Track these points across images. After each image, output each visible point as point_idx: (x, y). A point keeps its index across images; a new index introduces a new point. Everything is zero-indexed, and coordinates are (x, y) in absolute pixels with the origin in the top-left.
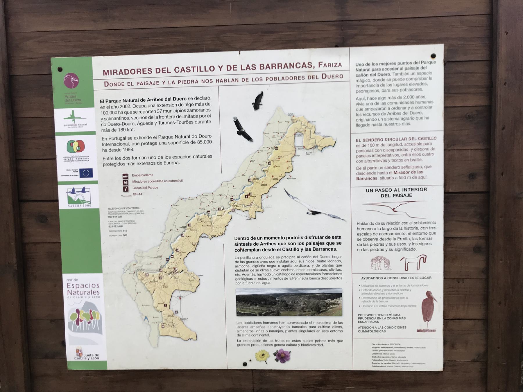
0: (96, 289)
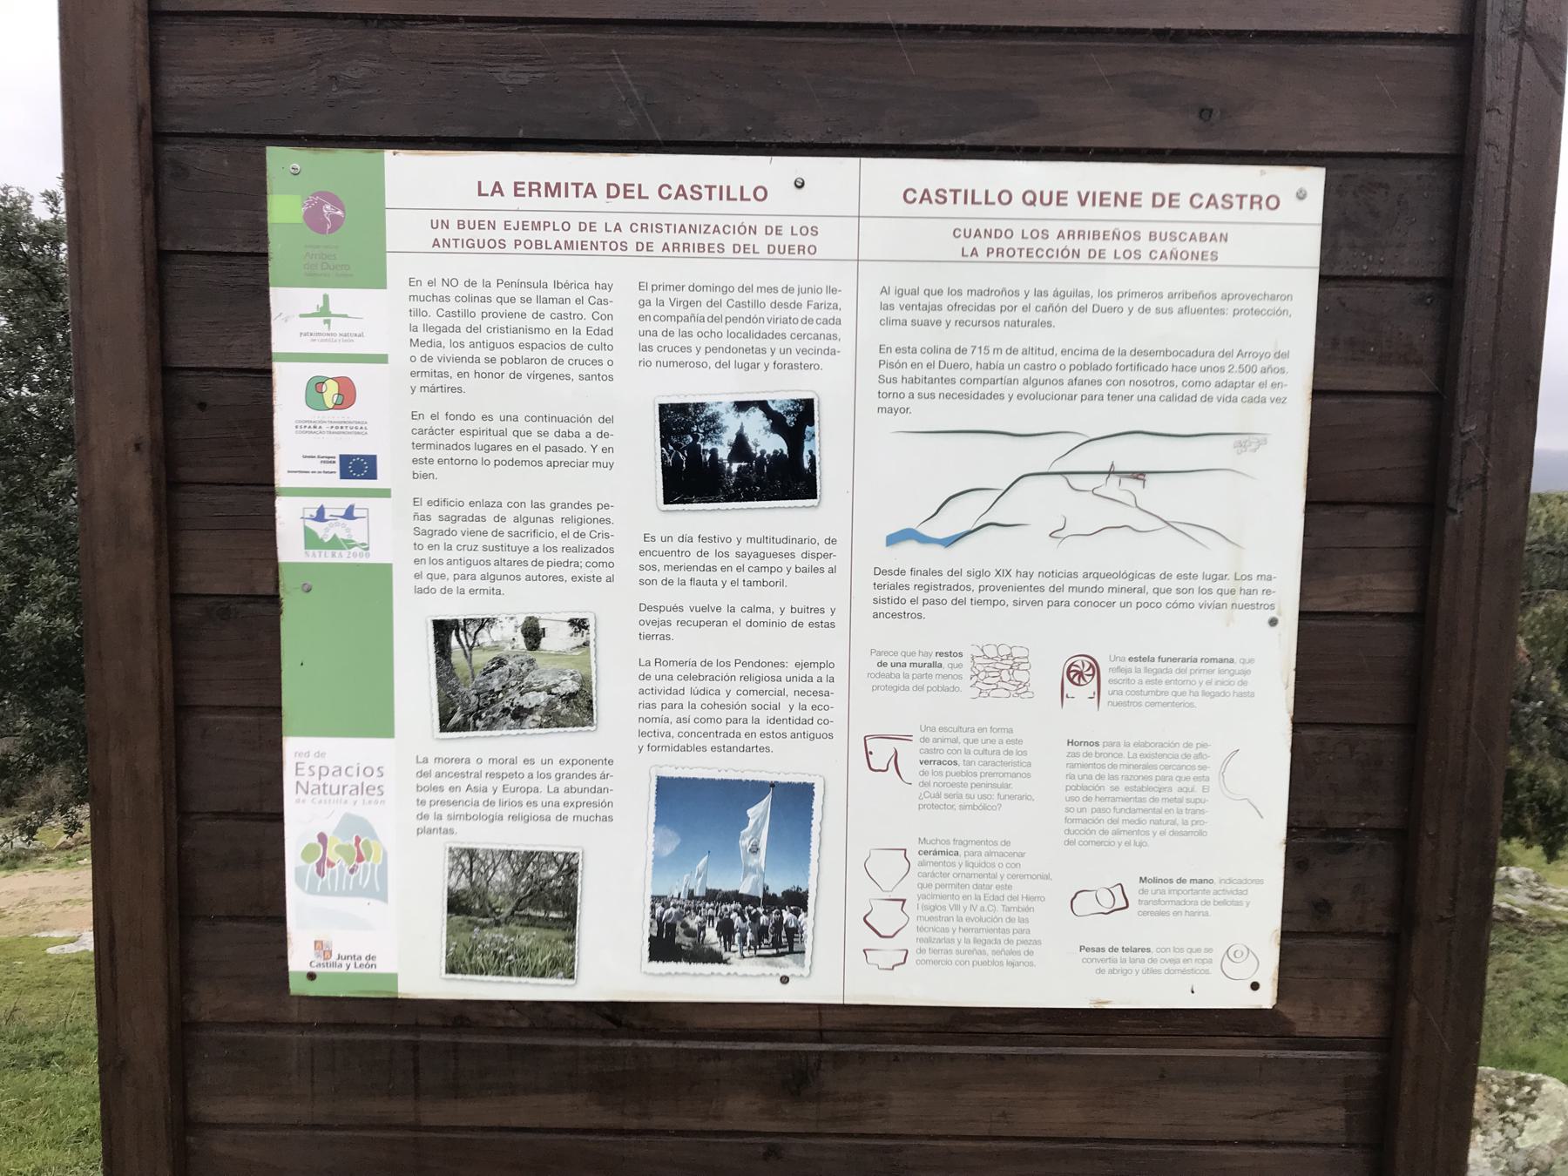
0: (374, 781)
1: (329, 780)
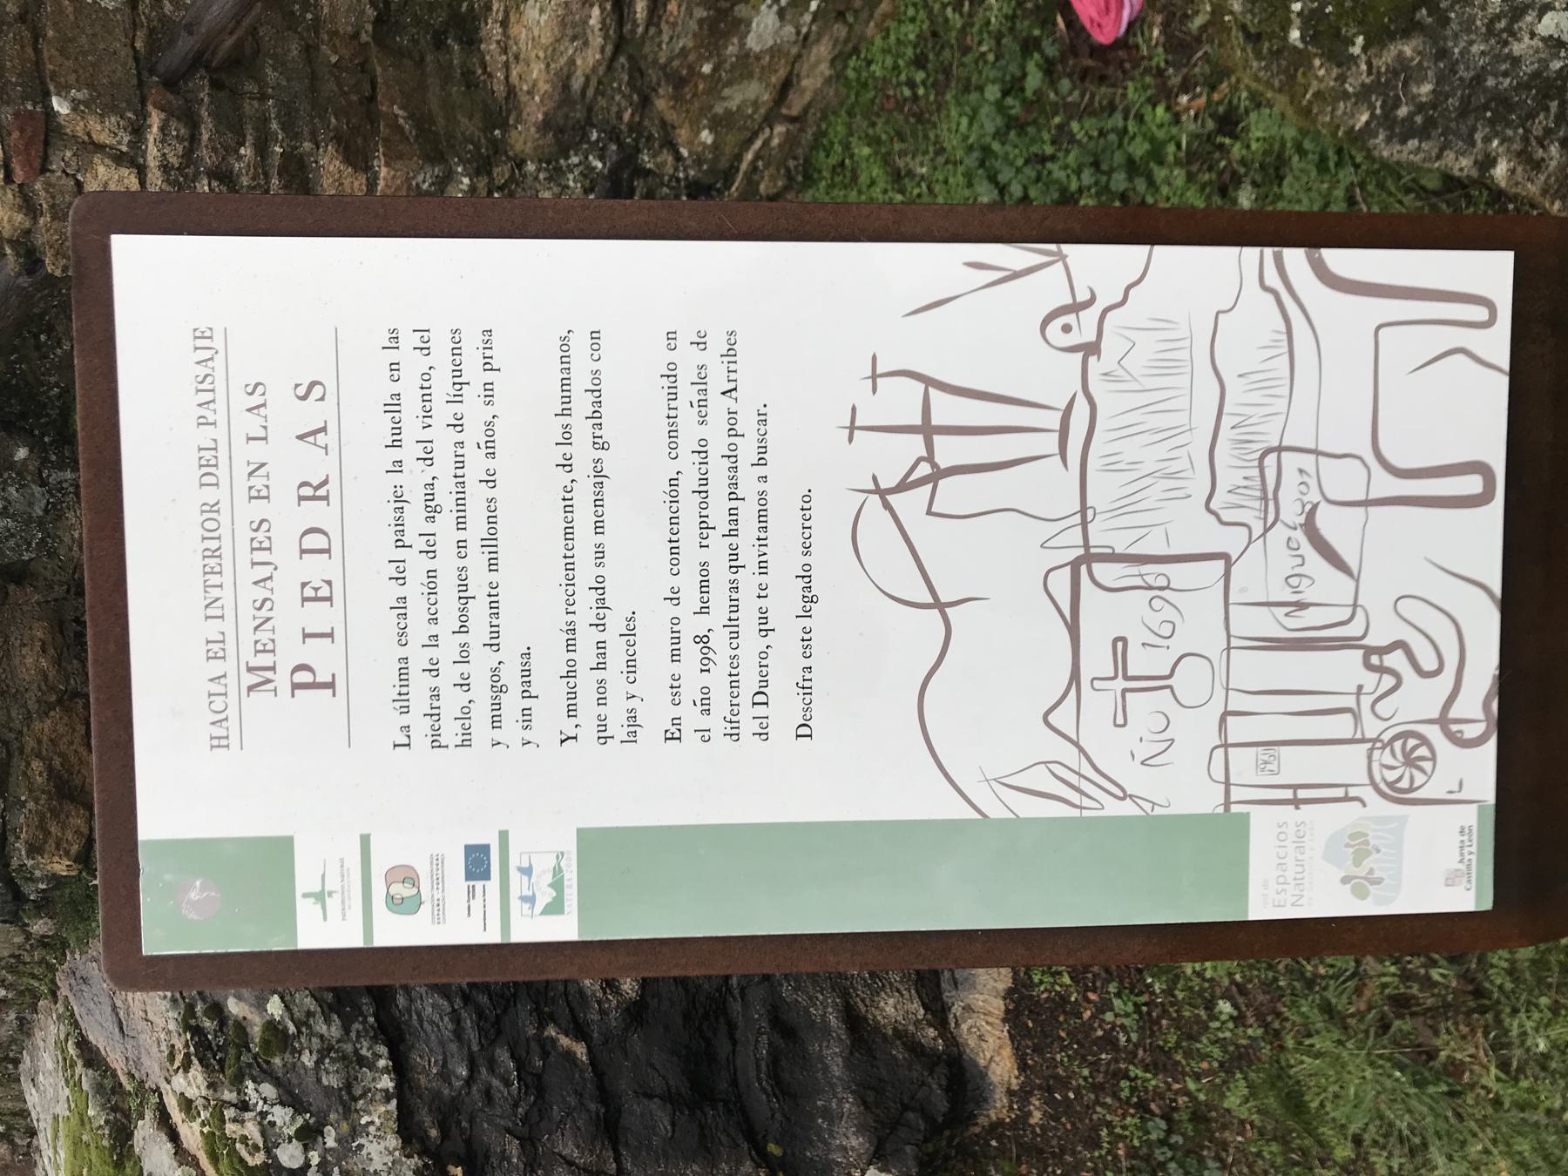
1: (1290, 875)
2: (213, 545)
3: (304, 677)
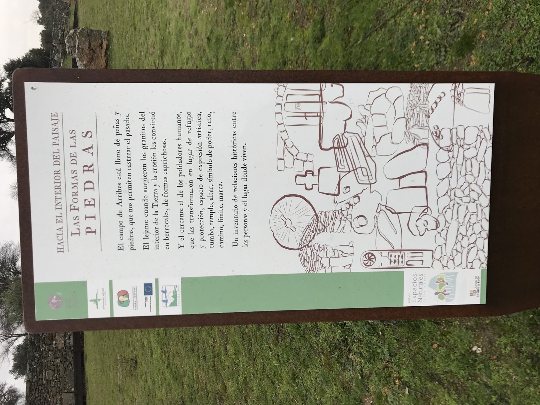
0: (418, 277)
1: (417, 292)
2: (58, 184)
3: (89, 230)
